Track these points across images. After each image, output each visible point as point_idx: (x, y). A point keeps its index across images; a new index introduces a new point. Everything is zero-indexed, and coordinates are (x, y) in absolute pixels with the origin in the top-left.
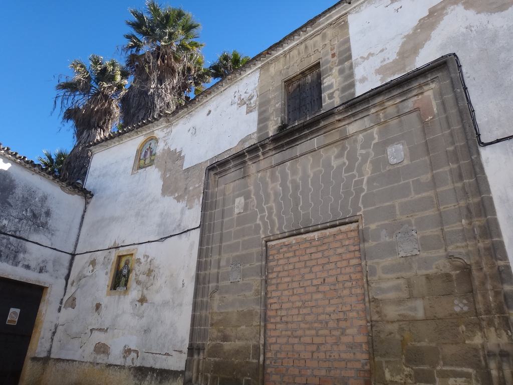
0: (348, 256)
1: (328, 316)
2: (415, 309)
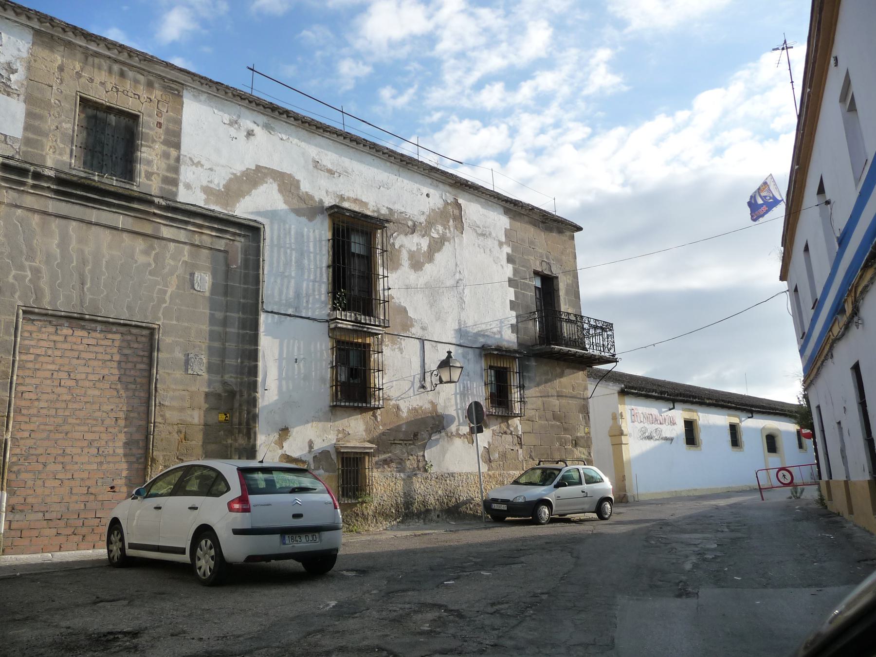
0: (135, 359)
1: (104, 414)
2: (192, 417)
